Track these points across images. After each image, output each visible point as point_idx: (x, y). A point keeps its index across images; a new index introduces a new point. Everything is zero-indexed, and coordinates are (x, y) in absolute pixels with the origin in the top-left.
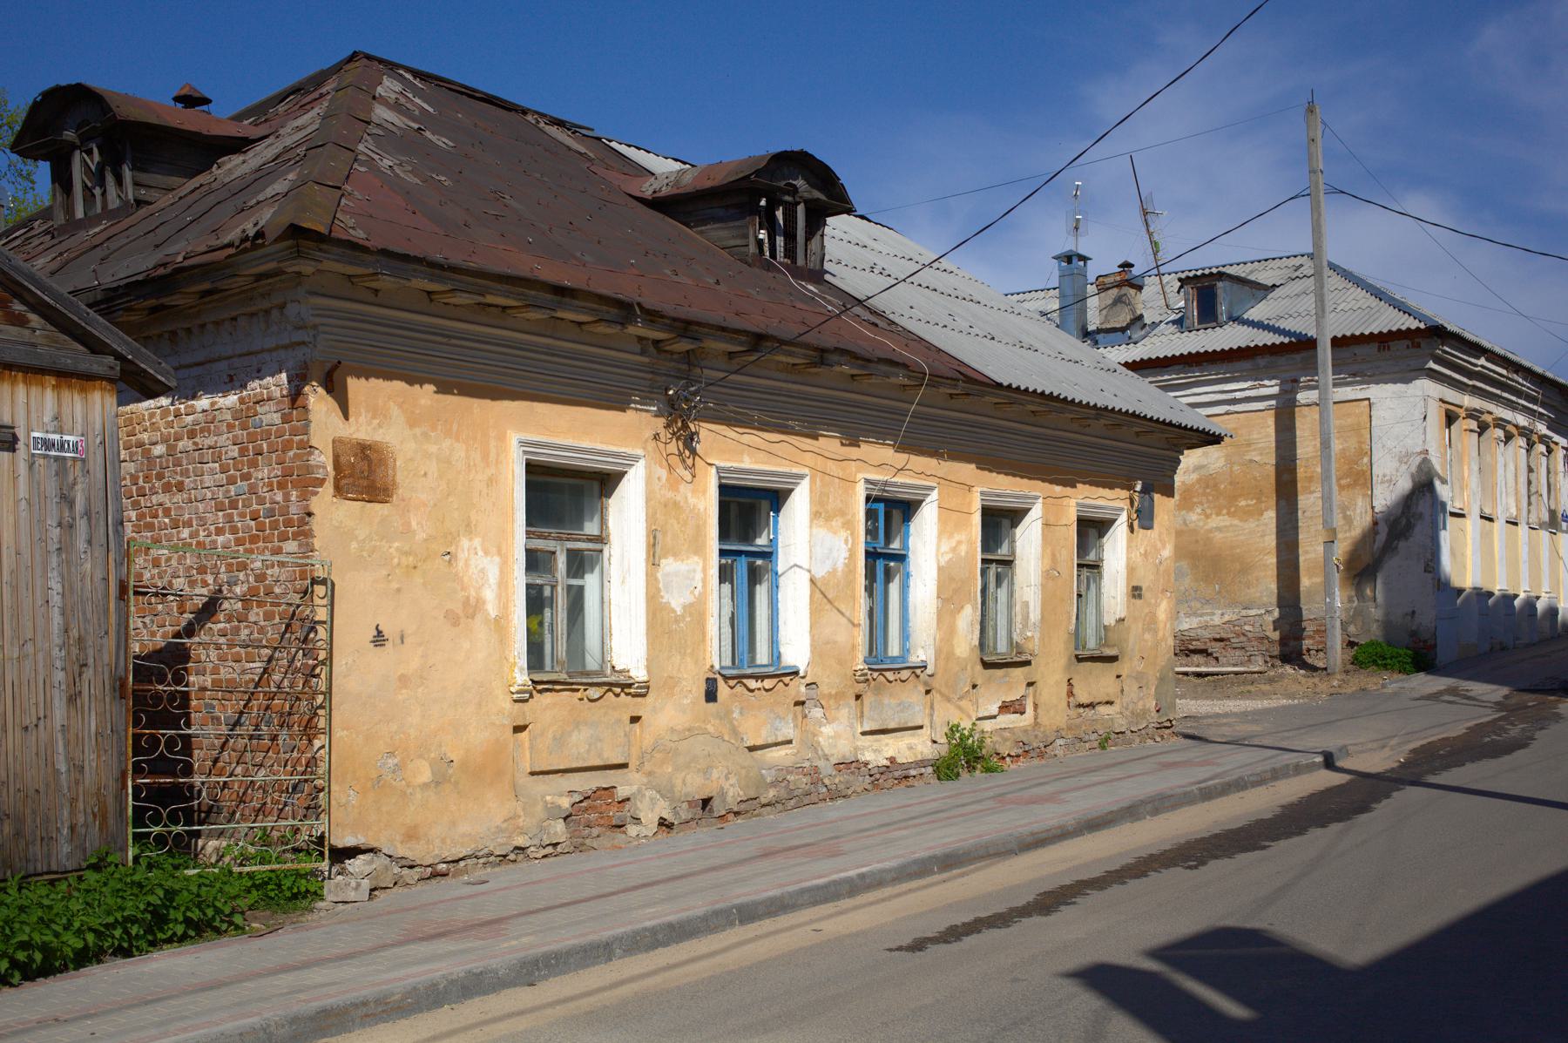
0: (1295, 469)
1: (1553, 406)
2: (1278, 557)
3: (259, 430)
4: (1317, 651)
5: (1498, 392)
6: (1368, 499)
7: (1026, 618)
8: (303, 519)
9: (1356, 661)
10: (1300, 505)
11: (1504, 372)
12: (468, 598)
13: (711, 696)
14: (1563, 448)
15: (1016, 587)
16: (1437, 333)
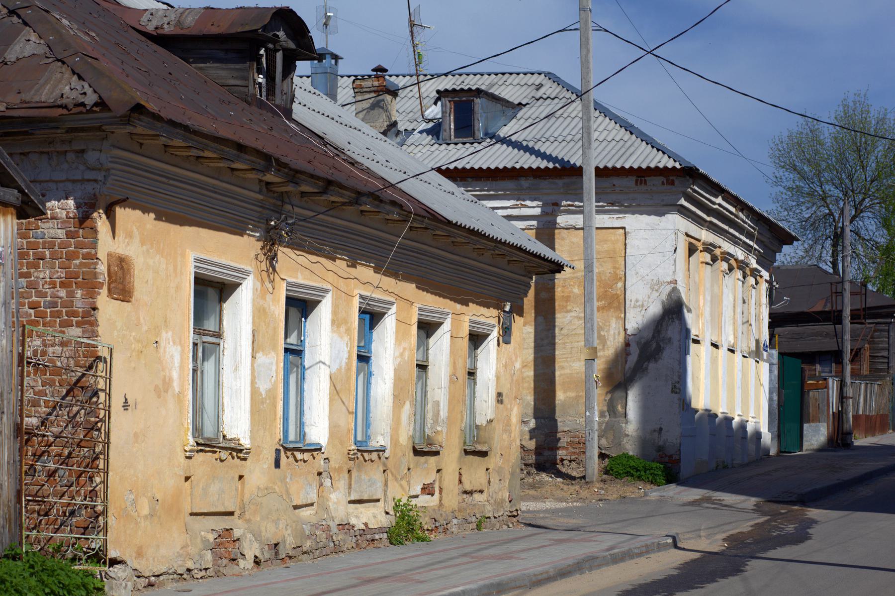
0: (553, 288)
1: (762, 242)
2: (535, 370)
3: (41, 241)
4: (570, 461)
5: (726, 227)
6: (621, 322)
7: (437, 414)
8: (89, 312)
9: (607, 472)
10: (558, 322)
11: (733, 210)
12: (165, 376)
13: (277, 464)
14: (766, 281)
15: (429, 389)
16: (690, 173)
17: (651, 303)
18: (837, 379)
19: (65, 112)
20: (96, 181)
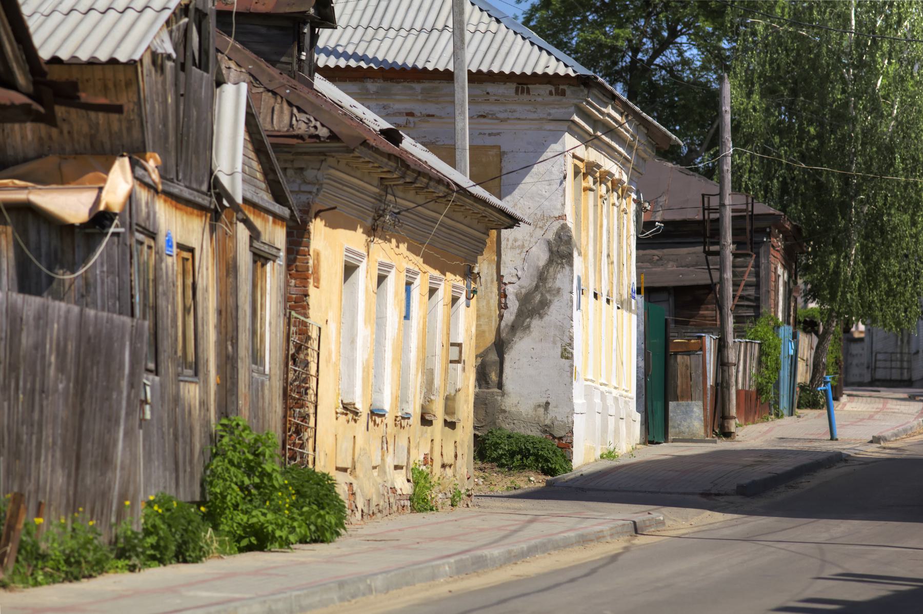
18: (714, 337)
19: (300, 141)
20: (310, 193)
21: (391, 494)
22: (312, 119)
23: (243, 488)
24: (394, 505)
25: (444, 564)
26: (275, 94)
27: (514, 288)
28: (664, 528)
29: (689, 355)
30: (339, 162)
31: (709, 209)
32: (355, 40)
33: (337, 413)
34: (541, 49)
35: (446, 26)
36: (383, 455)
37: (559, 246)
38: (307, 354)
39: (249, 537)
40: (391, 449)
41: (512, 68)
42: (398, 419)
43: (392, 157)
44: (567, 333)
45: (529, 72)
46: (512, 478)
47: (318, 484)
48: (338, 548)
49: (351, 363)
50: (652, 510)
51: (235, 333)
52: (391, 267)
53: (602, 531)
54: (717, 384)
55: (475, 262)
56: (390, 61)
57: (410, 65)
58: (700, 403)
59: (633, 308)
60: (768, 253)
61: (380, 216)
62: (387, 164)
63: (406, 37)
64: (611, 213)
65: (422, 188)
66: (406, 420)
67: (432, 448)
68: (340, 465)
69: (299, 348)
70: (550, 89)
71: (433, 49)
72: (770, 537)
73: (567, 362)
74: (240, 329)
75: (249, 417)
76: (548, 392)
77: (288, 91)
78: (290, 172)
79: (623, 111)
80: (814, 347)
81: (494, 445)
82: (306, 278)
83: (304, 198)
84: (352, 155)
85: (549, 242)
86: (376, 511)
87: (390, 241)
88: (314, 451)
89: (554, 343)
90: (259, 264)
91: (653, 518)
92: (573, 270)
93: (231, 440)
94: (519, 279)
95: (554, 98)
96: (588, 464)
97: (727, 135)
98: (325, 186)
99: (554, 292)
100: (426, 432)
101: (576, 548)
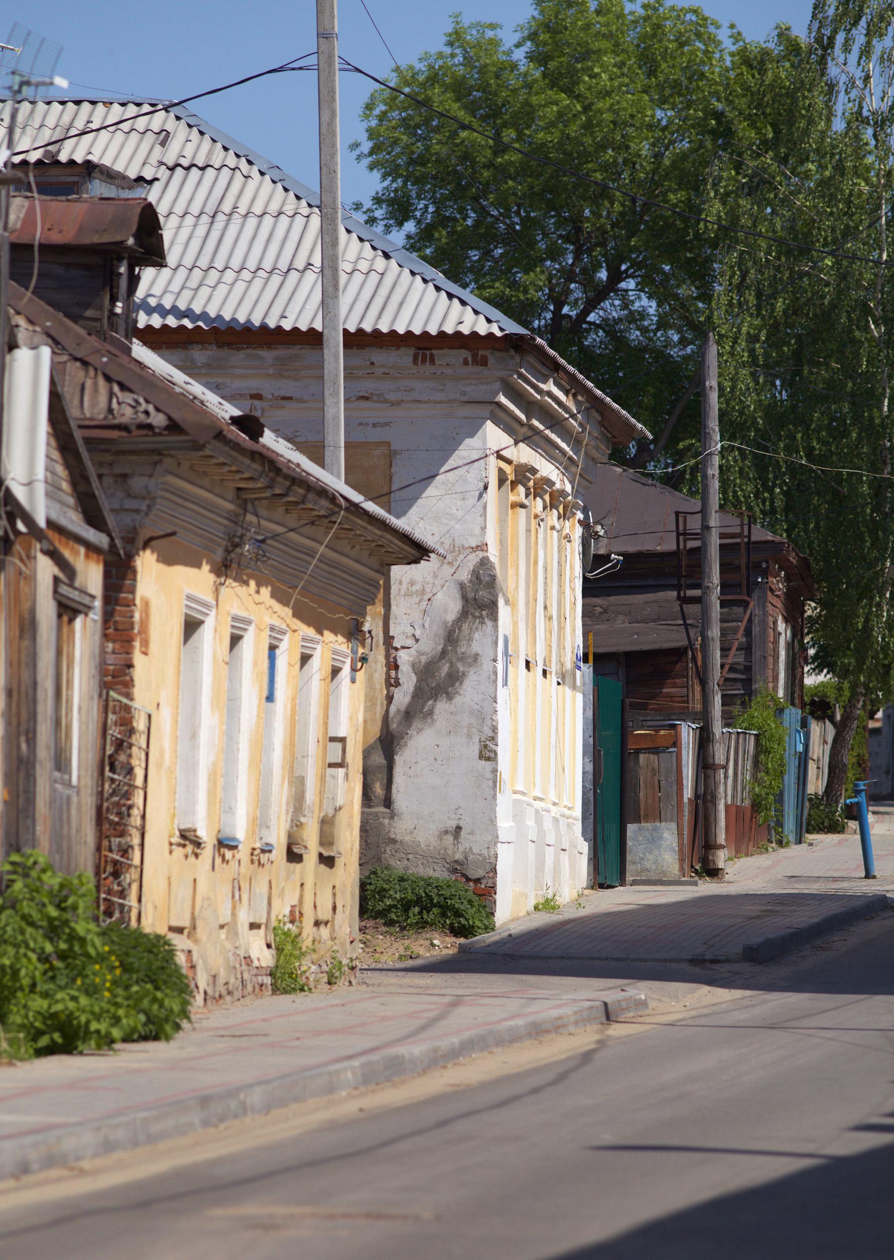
17: (439, 588)
18: (694, 726)
19: (124, 434)
20: (137, 511)
21: (244, 967)
22: (141, 400)
23: (44, 958)
24: (248, 983)
25: (345, 1069)
26: (85, 363)
27: (410, 656)
28: (647, 1012)
29: (657, 753)
30: (179, 464)
31: (685, 534)
32: (175, 287)
33: (171, 844)
34: (450, 296)
35: (310, 264)
36: (234, 908)
37: (477, 590)
38: (130, 756)
39: (50, 1033)
40: (245, 897)
41: (408, 326)
42: (256, 853)
43: (257, 456)
44: (488, 722)
45: (433, 331)
46: (407, 942)
47: (150, 952)
48: (182, 1048)
49: (191, 767)
50: (625, 985)
51: (32, 724)
52: (249, 622)
53: (560, 1018)
54: (697, 796)
55: (364, 615)
56: (227, 317)
57: (257, 323)
58: (674, 826)
59: (578, 683)
60: (763, 601)
61: (236, 546)
62: (249, 467)
63: (250, 282)
64: (549, 540)
65: (296, 503)
66: (267, 855)
67: (301, 897)
68: (174, 924)
69: (120, 745)
70: (464, 356)
71: (290, 299)
72: (806, 1023)
73: (488, 765)
74: (40, 717)
75: (50, 852)
76: (460, 811)
77: (105, 359)
78: (108, 481)
79: (569, 387)
80: (830, 740)
81: (379, 893)
82: (129, 641)
83: (127, 519)
84: (201, 453)
85: (462, 586)
86: (224, 993)
87: (246, 583)
88: (140, 901)
89: (469, 736)
90: (65, 618)
91: (631, 997)
92: (497, 627)
93: (26, 886)
94: (417, 641)
95: (470, 369)
96: (518, 919)
97: (713, 424)
98: (159, 500)
99: (469, 660)
100: (294, 872)
101: (527, 1043)
